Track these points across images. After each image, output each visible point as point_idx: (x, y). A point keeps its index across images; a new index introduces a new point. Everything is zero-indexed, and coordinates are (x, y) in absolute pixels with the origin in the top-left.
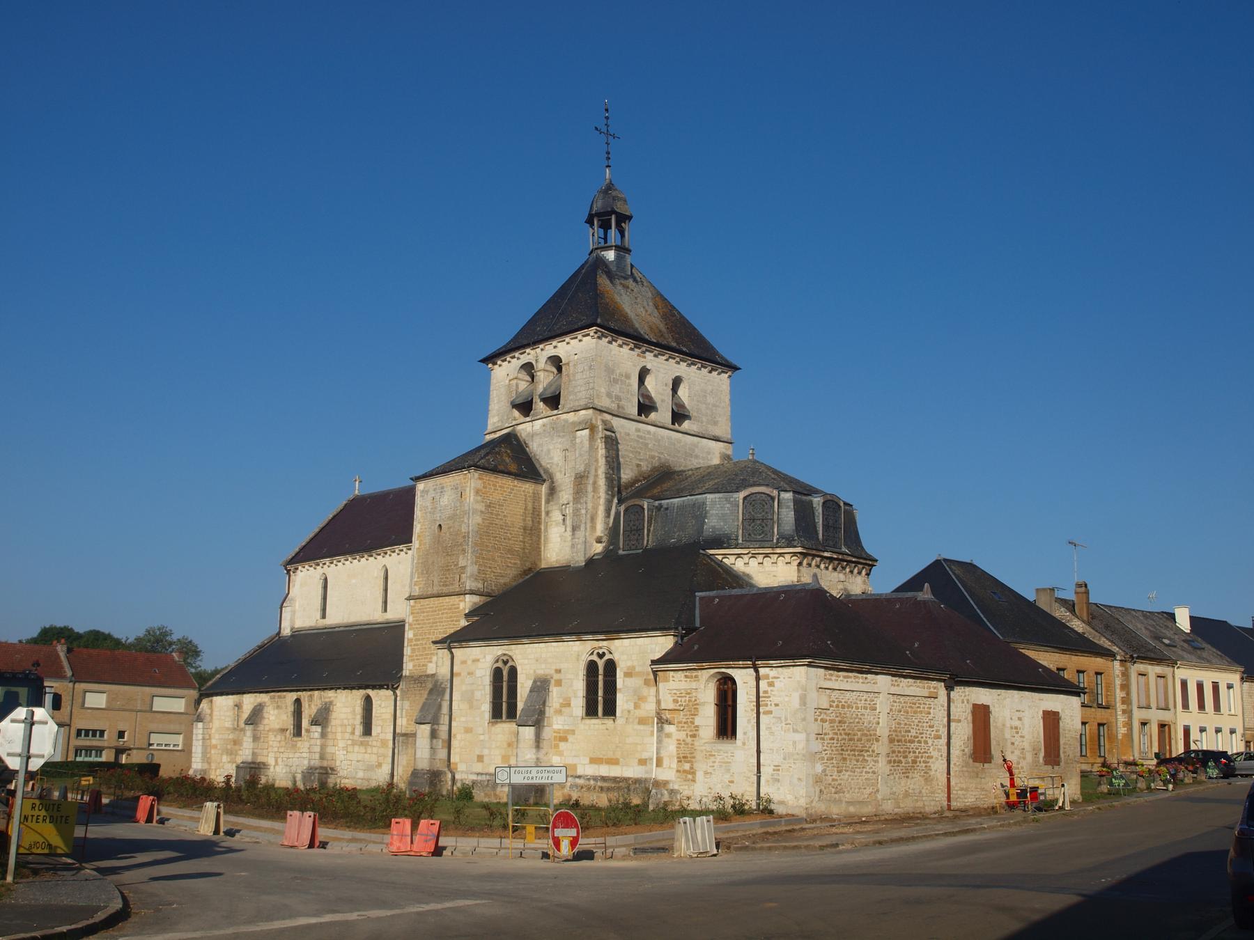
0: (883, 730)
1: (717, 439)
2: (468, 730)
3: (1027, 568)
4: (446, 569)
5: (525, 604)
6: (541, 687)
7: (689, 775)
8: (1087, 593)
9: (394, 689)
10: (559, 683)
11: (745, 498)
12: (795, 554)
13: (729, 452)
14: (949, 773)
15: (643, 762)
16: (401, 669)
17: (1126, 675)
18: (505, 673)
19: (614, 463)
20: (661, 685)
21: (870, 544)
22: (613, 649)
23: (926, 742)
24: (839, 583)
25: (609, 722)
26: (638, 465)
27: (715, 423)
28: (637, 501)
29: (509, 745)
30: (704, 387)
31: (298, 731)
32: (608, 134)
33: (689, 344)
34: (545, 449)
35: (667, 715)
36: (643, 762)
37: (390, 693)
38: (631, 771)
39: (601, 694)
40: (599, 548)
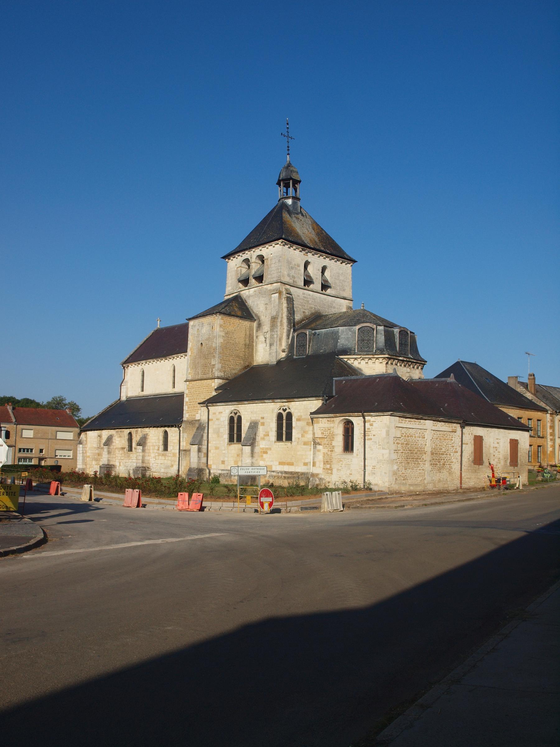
0: (428, 448)
1: (345, 298)
2: (217, 448)
3: (504, 368)
4: (205, 366)
5: (245, 384)
6: (254, 426)
7: (329, 471)
8: (534, 379)
9: (179, 427)
10: (263, 424)
11: (359, 329)
12: (384, 358)
13: (351, 305)
14: (461, 470)
15: (306, 464)
16: (183, 417)
17: (553, 421)
18: (236, 419)
19: (291, 311)
20: (315, 425)
21: (423, 354)
22: (290, 407)
23: (450, 455)
24: (407, 373)
25: (288, 444)
26: (304, 312)
27: (344, 290)
28: (303, 331)
29: (238, 455)
30: (338, 271)
31: (130, 449)
32: (288, 136)
33: (331, 249)
34: (256, 303)
35: (318, 441)
36: (306, 464)
37: (177, 429)
38: (299, 469)
39: (285, 429)
40: (283, 355)
